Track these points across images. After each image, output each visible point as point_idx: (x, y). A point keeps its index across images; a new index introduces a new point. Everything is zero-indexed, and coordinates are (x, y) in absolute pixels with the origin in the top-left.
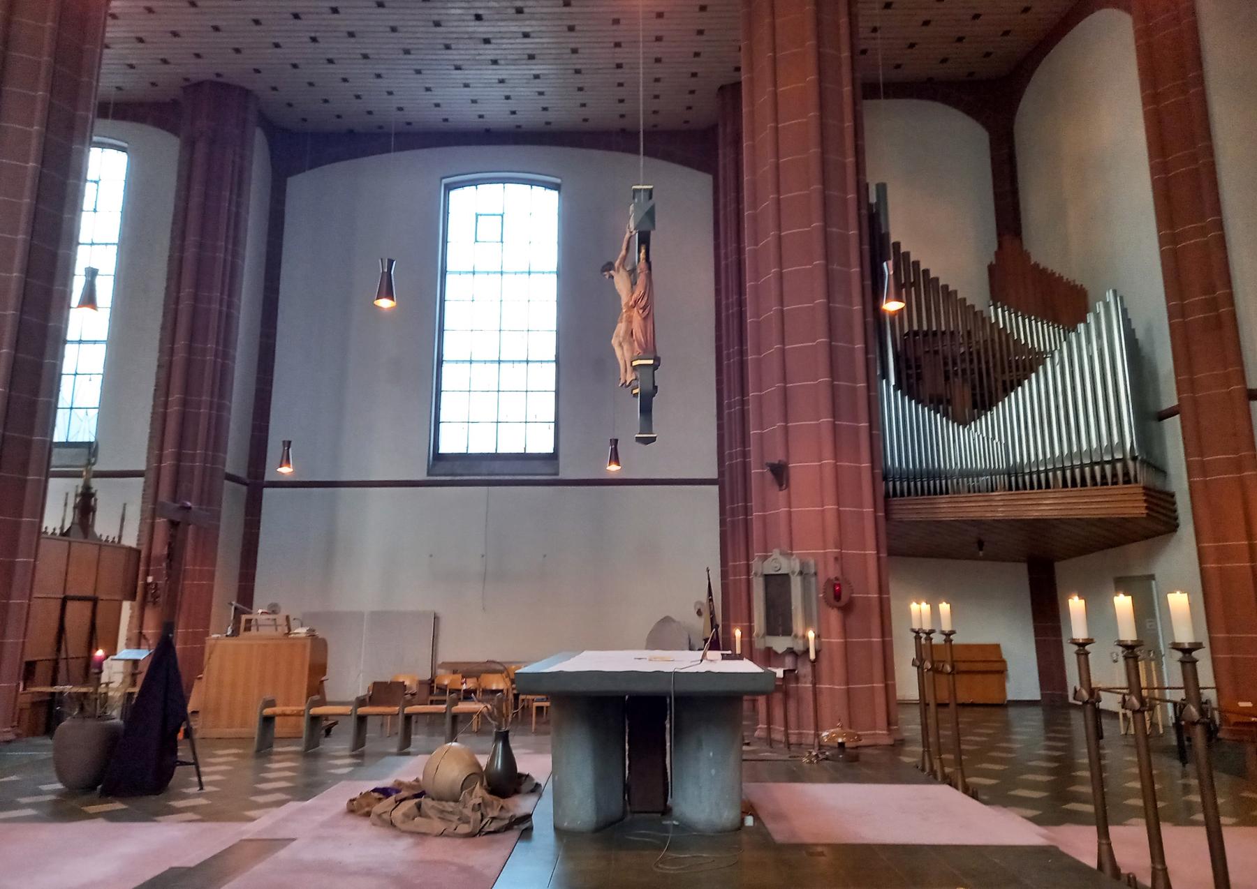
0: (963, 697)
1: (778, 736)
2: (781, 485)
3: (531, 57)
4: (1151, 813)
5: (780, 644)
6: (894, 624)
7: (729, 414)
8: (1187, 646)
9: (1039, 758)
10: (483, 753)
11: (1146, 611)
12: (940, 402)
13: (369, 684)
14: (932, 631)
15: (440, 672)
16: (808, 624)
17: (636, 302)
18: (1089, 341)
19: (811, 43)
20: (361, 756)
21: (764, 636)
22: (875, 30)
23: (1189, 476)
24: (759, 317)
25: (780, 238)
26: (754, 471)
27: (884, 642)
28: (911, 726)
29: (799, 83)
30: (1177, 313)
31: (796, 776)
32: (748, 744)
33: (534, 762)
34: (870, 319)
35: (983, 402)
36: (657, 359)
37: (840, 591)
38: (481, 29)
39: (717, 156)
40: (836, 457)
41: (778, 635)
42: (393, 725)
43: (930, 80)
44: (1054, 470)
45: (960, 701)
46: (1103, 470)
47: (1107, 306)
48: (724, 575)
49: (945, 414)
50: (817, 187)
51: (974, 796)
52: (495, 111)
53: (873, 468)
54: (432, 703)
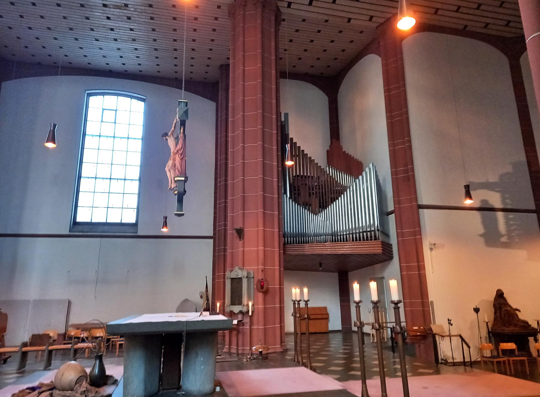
0: (312, 330)
1: (234, 351)
2: (240, 238)
3: (134, 40)
4: (382, 373)
5: (236, 309)
6: (285, 299)
9: (339, 359)
10: (88, 367)
11: (382, 289)
12: (307, 205)
13: (30, 335)
14: (300, 301)
15: (70, 329)
16: (249, 299)
17: (177, 151)
18: (363, 183)
19: (259, 51)
20: (23, 372)
22: (285, 50)
24: (233, 149)
26: (229, 232)
27: (280, 288)
28: (290, 343)
29: (254, 67)
30: (394, 174)
31: (240, 367)
32: (220, 355)
33: (115, 370)
35: (323, 205)
36: (186, 178)
37: (263, 285)
38: (110, 23)
39: (218, 95)
41: (236, 305)
42: (42, 356)
43: (306, 74)
44: (349, 234)
45: (310, 331)
46: (367, 235)
48: (214, 279)
49: (309, 210)
51: (314, 370)
53: (279, 231)
54: (64, 344)
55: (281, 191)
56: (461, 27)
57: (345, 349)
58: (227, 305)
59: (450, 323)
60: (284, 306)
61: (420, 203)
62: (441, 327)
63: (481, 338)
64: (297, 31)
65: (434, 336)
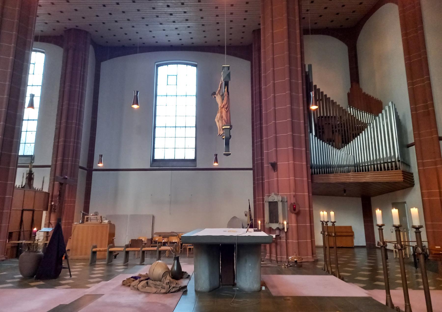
0: (339, 245)
1: (274, 258)
2: (274, 170)
3: (187, 20)
4: (405, 285)
5: (274, 226)
6: (314, 219)
7: (256, 145)
8: (417, 227)
9: (366, 266)
10: (170, 264)
11: (403, 214)
12: (331, 141)
13: (130, 240)
14: (328, 222)
15: (155, 236)
16: (284, 219)
17: (224, 106)
18: (383, 120)
19: (285, 15)
20: (127, 265)
21: (268, 223)
22: (308, 10)
23: (418, 167)
24: (267, 111)
25: (274, 83)
26: (265, 165)
27: (311, 225)
28: (320, 255)
29: (281, 29)
30: (414, 110)
31: (280, 272)
32: (263, 261)
33: (188, 268)
34: (306, 112)
35: (346, 141)
36: (231, 126)
37: (295, 207)
38: (169, 10)
39: (252, 55)
40: (294, 160)
41: (273, 223)
42: (138, 254)
43: (327, 28)
44: (371, 165)
45: (338, 246)
46: (388, 165)
47: (389, 107)
48: (255, 202)
49: (332, 145)
50: (287, 65)
51: (343, 279)
52: (174, 39)
53: (307, 164)
54: (152, 247)
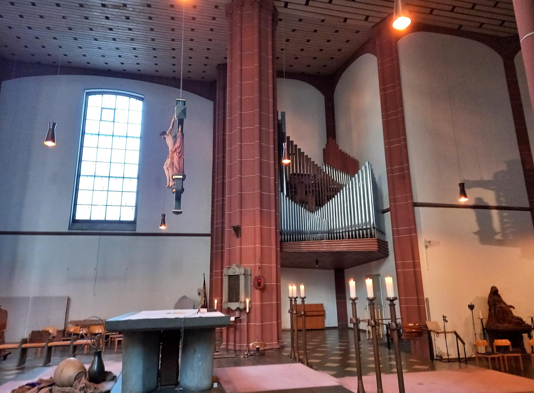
0: (308, 327)
1: (231, 347)
2: (237, 236)
3: (132, 40)
4: (378, 369)
5: (234, 306)
6: (282, 296)
9: (335, 355)
10: (87, 363)
11: (378, 286)
12: (303, 203)
13: (30, 332)
14: (297, 298)
15: (69, 326)
16: (246, 296)
17: (175, 150)
18: (359, 182)
19: (256, 50)
20: (23, 369)
22: (282, 50)
26: (227, 230)
27: (277, 285)
28: (287, 340)
29: (251, 66)
30: (390, 172)
31: (238, 363)
32: (218, 352)
33: (113, 366)
35: (320, 203)
36: (184, 176)
37: (260, 282)
38: (109, 23)
39: (215, 94)
41: (233, 302)
42: (42, 352)
43: (303, 73)
44: (345, 232)
45: (307, 328)
46: (363, 232)
48: (211, 277)
49: (305, 208)
51: (311, 367)
53: (276, 229)
54: (64, 340)
55: (278, 189)
56: (456, 27)
57: (341, 346)
58: (224, 302)
59: (445, 320)
60: (280, 303)
61: (415, 201)
62: (436, 323)
63: (475, 334)
64: (294, 30)
65: (429, 332)
